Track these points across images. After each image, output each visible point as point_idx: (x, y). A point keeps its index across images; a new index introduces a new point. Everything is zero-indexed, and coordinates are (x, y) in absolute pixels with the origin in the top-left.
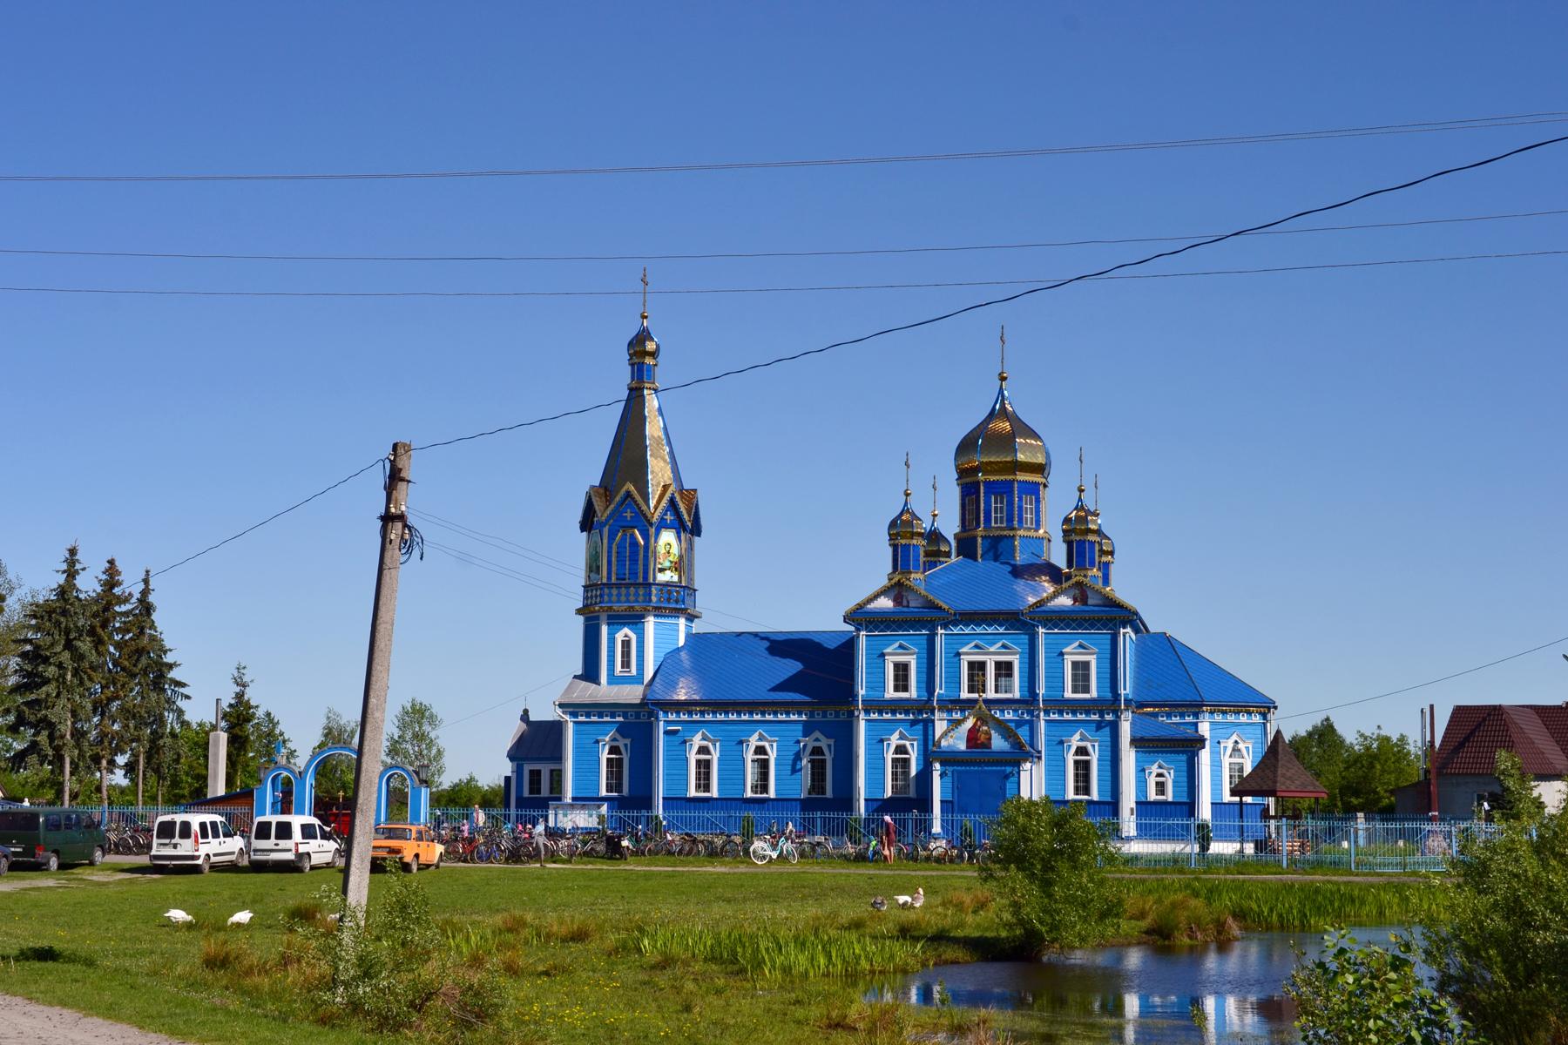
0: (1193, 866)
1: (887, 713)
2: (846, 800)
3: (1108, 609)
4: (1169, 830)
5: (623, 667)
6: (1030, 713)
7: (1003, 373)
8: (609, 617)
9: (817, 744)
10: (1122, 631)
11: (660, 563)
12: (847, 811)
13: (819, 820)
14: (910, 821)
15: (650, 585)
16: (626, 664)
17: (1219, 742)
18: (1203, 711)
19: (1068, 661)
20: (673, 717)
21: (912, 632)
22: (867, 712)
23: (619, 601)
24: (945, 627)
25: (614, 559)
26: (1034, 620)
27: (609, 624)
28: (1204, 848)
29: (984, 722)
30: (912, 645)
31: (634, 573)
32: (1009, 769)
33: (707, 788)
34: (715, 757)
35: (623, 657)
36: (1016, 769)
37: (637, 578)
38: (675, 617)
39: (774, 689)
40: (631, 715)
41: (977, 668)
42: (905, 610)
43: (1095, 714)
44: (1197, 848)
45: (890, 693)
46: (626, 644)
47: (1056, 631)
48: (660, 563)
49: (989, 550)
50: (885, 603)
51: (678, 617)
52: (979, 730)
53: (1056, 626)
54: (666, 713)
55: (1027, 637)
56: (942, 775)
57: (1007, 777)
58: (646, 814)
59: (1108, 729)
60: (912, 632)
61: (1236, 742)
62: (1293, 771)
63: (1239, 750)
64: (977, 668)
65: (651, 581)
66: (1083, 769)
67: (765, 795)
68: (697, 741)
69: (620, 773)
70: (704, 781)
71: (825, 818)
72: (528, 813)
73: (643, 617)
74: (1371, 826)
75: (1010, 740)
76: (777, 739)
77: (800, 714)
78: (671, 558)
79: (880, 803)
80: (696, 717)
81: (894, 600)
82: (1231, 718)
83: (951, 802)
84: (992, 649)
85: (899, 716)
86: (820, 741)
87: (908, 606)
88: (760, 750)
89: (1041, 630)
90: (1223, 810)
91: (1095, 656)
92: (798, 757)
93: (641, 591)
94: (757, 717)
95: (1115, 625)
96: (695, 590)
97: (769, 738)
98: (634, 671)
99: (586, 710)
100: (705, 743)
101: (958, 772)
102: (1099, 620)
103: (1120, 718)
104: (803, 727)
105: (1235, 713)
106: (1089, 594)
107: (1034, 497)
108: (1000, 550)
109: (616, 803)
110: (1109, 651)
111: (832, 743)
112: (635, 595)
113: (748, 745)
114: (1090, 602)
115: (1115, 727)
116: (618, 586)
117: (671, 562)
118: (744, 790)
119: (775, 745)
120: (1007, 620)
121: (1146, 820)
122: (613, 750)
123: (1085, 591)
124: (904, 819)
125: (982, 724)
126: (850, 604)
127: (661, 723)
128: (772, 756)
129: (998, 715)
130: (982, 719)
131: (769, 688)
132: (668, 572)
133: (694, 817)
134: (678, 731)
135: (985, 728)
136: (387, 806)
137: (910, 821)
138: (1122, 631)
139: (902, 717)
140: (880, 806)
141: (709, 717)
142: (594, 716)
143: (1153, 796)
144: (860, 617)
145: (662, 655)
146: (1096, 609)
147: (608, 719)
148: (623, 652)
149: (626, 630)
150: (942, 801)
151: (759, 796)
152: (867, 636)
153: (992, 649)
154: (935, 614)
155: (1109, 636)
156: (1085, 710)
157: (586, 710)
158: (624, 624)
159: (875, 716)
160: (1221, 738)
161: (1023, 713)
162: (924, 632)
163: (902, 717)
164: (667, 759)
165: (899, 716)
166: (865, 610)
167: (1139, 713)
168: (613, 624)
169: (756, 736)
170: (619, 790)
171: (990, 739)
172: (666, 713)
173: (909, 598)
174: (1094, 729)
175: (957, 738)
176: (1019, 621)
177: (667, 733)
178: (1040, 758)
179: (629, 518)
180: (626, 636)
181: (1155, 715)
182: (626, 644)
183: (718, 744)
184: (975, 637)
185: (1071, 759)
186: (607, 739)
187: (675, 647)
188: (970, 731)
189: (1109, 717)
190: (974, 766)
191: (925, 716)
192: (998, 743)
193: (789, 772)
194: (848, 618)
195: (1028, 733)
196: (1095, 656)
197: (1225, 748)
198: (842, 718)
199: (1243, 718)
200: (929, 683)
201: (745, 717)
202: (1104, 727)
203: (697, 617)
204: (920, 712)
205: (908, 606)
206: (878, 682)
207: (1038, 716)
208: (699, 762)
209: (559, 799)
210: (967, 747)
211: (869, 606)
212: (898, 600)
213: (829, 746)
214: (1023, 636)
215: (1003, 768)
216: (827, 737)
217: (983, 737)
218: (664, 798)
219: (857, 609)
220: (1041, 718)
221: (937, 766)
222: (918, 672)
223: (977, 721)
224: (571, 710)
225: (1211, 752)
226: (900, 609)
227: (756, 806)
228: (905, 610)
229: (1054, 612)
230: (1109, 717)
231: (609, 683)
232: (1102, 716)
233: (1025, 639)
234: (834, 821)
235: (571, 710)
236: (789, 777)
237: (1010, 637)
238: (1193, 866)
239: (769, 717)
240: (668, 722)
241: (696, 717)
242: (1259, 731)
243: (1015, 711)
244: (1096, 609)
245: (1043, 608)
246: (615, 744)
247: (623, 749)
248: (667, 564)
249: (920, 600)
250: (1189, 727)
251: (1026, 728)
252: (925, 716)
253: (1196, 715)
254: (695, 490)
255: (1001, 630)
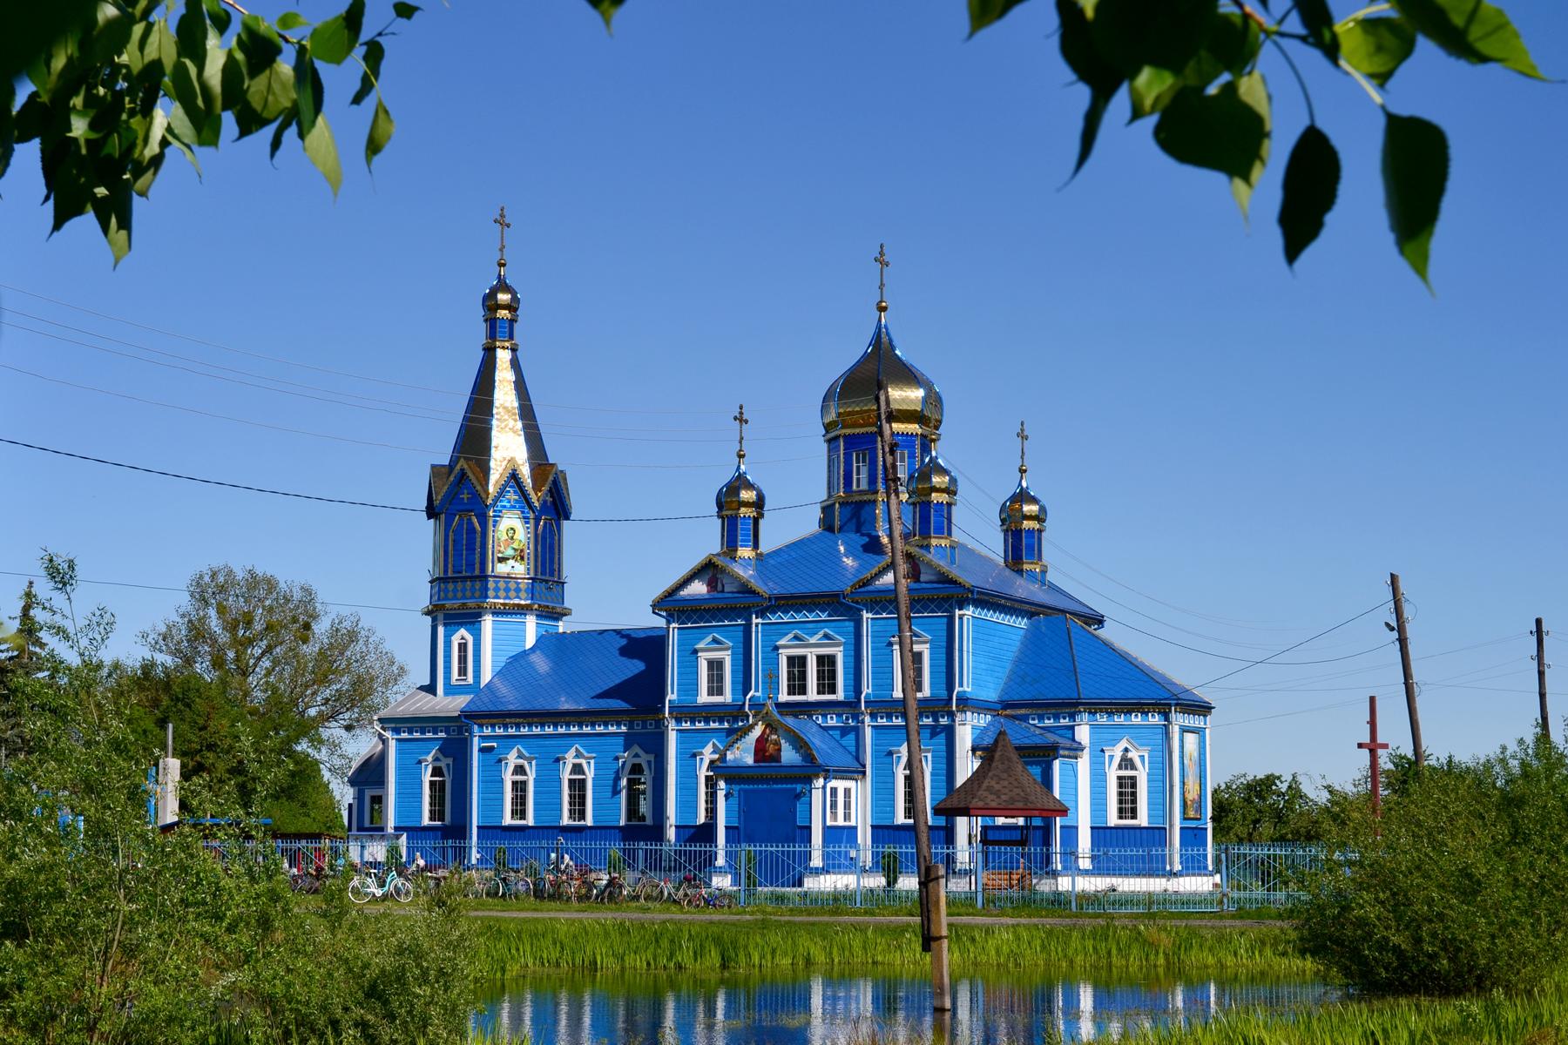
0: (858, 905)
1: (700, 722)
2: (656, 832)
3: (940, 586)
4: (1193, 862)
5: (460, 675)
6: (855, 717)
7: (881, 302)
8: (447, 617)
9: (637, 761)
10: (957, 612)
11: (500, 552)
12: (460, 839)
13: (450, 850)
14: (450, 850)
15: (487, 577)
16: (463, 671)
17: (1103, 751)
18: (1080, 712)
19: (784, 654)
20: (488, 731)
21: (726, 623)
22: (679, 721)
23: (455, 598)
24: (761, 614)
25: (450, 547)
26: (857, 603)
27: (445, 625)
28: (891, 882)
29: (774, 730)
30: (839, 634)
31: (471, 565)
32: (799, 787)
33: (523, 815)
34: (531, 777)
35: (460, 663)
36: (808, 787)
37: (474, 570)
38: (521, 614)
39: (600, 696)
40: (454, 731)
41: (797, 663)
42: (720, 595)
43: (927, 717)
44: (883, 881)
45: (704, 698)
46: (463, 647)
47: (884, 615)
48: (500, 552)
49: (850, 520)
50: (698, 588)
51: (525, 615)
52: (767, 739)
53: (689, 619)
54: (481, 726)
55: (852, 624)
56: (727, 796)
57: (798, 796)
58: (747, 848)
59: (943, 735)
60: (726, 623)
61: (1126, 750)
62: (1006, 783)
63: (1131, 760)
64: (797, 663)
65: (490, 573)
66: (1127, 788)
67: (582, 823)
68: (512, 759)
69: (442, 798)
70: (519, 810)
71: (455, 847)
72: (708, 849)
73: (480, 615)
74: (1101, 853)
75: (802, 751)
76: (594, 755)
77: (619, 724)
78: (515, 545)
79: (692, 830)
80: (512, 731)
81: (709, 585)
82: (1120, 719)
83: (736, 828)
84: (813, 640)
85: (712, 725)
86: (639, 756)
87: (723, 591)
88: (577, 769)
89: (866, 615)
90: (1126, 836)
91: (928, 646)
92: (617, 779)
93: (478, 585)
94: (574, 730)
95: (951, 606)
96: (563, 583)
97: (586, 754)
98: (470, 679)
99: (409, 725)
100: (520, 761)
101: (746, 791)
102: (932, 600)
103: (954, 721)
104: (625, 740)
105: (1125, 714)
106: (923, 569)
107: (906, 452)
108: (862, 520)
109: (440, 833)
110: (945, 639)
111: (653, 760)
112: (462, 591)
113: (702, 759)
114: (923, 578)
115: (950, 732)
116: (454, 580)
117: (515, 550)
118: (561, 817)
119: (592, 762)
120: (829, 604)
121: (895, 848)
122: (437, 772)
123: (918, 565)
124: (634, 850)
125: (771, 733)
126: (658, 590)
127: (476, 740)
128: (590, 775)
129: (820, 722)
130: (771, 726)
131: (594, 694)
132: (511, 562)
133: (700, 851)
134: (492, 748)
135: (774, 737)
136: (1213, 836)
137: (640, 851)
138: (957, 612)
139: (716, 725)
140: (695, 833)
141: (524, 731)
142: (417, 732)
143: (1113, 820)
144: (670, 604)
145: (504, 659)
146: (929, 586)
147: (429, 735)
148: (460, 657)
149: (463, 631)
150: (727, 828)
151: (577, 823)
152: (678, 628)
153: (813, 640)
154: (750, 600)
155: (945, 620)
156: (887, 713)
157: (409, 725)
158: (461, 625)
159: (686, 725)
160: (1106, 746)
161: (847, 719)
162: (739, 622)
163: (716, 725)
164: (481, 781)
165: (712, 725)
166: (677, 597)
167: (1007, 716)
168: (450, 624)
169: (572, 752)
170: (442, 819)
171: (779, 750)
172: (481, 726)
173: (724, 582)
174: (929, 735)
175: (745, 751)
176: (842, 604)
177: (482, 750)
178: (864, 773)
179: (466, 501)
180: (463, 638)
181: (1024, 718)
182: (463, 647)
183: (534, 763)
184: (822, 624)
185: (1113, 775)
186: (430, 758)
187: (521, 650)
188: (758, 740)
189: (944, 721)
190: (763, 784)
191: (740, 724)
192: (789, 755)
193: (610, 794)
194: (657, 606)
195: (854, 742)
196: (928, 646)
197: (1111, 757)
198: (651, 728)
199: (1136, 719)
200: (948, 675)
201: (561, 730)
202: (940, 733)
203: (566, 615)
204: (736, 720)
205: (723, 591)
206: (690, 686)
207: (863, 722)
208: (514, 783)
209: (382, 829)
210: (755, 761)
211: (682, 593)
212: (712, 585)
213: (649, 762)
214: (847, 623)
215: (794, 786)
216: (647, 752)
217: (771, 748)
218: (479, 827)
219: (666, 597)
220: (866, 724)
221: (722, 784)
222: (733, 672)
223: (765, 728)
224: (393, 725)
225: (1092, 763)
226: (716, 595)
227: (573, 835)
228: (720, 595)
229: (880, 591)
230: (944, 721)
231: (446, 693)
232: (936, 720)
233: (850, 626)
234: (656, 853)
235: (393, 725)
236: (608, 801)
237: (833, 624)
238: (858, 905)
239: (587, 730)
240: (483, 738)
241: (512, 731)
242: (1159, 738)
243: (840, 716)
244: (929, 586)
245: (869, 588)
246: (438, 764)
247: (445, 770)
248: (510, 552)
249: (736, 584)
250: (1065, 731)
251: (852, 736)
252: (740, 724)
253: (1072, 716)
254: (433, 467)
255: (824, 617)
